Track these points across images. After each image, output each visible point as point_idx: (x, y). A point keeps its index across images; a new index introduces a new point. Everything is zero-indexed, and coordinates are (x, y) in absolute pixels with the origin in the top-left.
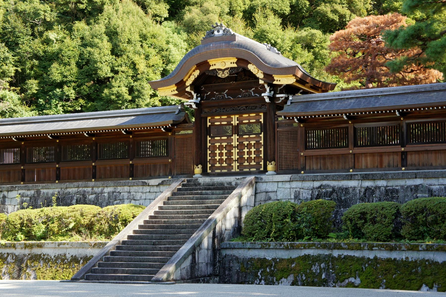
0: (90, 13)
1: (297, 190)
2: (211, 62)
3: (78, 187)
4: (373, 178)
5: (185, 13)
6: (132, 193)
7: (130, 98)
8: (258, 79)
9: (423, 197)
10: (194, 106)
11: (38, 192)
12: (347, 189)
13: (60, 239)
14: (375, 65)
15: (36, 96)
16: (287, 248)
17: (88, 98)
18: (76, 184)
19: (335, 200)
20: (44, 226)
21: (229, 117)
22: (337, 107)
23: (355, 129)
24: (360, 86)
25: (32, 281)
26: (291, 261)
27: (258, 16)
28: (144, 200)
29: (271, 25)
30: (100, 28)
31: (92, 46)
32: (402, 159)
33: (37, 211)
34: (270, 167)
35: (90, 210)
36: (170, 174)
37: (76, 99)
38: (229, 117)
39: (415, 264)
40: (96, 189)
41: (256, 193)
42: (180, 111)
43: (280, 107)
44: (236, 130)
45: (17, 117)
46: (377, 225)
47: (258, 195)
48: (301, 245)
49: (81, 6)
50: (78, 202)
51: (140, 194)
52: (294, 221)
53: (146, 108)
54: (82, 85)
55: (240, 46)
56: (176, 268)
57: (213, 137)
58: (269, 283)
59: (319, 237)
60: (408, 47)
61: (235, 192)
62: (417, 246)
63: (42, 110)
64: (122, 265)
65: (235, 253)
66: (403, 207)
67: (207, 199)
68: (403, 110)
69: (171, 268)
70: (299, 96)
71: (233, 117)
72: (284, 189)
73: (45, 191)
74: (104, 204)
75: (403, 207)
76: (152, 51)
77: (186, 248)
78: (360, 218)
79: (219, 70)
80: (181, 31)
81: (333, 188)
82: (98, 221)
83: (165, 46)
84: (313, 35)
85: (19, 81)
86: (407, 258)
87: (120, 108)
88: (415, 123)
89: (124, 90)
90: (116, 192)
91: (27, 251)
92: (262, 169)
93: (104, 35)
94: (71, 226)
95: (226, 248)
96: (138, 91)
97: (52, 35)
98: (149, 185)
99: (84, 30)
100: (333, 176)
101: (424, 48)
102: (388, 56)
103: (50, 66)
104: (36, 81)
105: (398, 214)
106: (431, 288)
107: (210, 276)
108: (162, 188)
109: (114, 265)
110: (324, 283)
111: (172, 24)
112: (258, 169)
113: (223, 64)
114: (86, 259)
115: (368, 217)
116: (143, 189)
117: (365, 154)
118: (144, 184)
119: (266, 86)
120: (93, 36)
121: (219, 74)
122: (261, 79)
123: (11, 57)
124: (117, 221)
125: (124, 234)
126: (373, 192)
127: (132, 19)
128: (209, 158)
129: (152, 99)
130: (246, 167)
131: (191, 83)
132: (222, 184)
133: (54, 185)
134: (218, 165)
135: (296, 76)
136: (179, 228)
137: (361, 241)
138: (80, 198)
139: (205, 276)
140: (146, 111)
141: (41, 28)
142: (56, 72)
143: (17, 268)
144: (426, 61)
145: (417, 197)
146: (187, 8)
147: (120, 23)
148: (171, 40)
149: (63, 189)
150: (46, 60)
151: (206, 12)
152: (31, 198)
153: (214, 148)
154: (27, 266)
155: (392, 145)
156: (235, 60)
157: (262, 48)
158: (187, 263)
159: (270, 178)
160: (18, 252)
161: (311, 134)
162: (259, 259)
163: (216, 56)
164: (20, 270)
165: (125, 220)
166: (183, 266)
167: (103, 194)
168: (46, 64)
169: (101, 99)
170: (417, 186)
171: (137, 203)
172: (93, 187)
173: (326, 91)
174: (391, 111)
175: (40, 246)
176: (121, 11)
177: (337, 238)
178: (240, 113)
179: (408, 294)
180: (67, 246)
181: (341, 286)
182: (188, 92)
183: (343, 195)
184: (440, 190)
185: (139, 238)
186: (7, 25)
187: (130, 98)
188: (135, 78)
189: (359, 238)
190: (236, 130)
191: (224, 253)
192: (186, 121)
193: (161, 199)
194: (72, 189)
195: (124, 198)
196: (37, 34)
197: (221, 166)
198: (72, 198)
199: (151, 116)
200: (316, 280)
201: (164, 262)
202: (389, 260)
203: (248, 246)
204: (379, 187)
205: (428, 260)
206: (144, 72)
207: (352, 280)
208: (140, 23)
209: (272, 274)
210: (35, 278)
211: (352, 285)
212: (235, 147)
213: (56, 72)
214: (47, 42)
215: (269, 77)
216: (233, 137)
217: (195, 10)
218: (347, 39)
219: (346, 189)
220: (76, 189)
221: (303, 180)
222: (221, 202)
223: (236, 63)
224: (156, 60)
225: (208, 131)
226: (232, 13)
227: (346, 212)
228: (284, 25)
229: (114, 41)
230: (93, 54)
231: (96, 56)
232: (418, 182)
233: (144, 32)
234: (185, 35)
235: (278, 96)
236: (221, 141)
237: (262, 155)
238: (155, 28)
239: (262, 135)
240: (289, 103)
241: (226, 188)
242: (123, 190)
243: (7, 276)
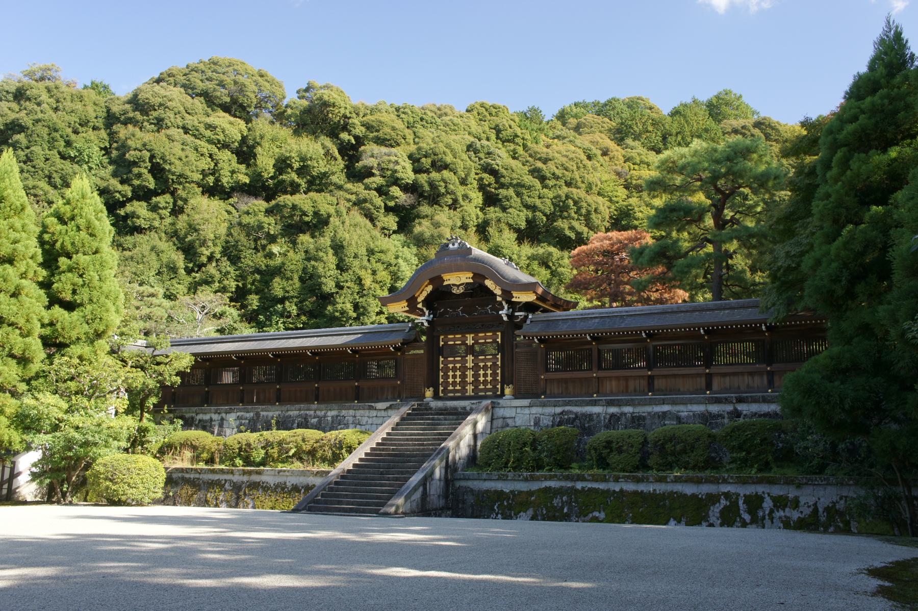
0: (315, 226)
2: (445, 277)
3: (300, 410)
4: (618, 404)
5: (414, 226)
7: (355, 315)
8: (495, 295)
9: (670, 424)
10: (426, 324)
11: (258, 414)
13: (280, 466)
14: (619, 283)
15: (256, 313)
16: (526, 480)
17: (311, 314)
18: (297, 406)
19: (578, 427)
20: (263, 452)
21: (463, 336)
22: (580, 327)
23: (599, 351)
25: (250, 510)
26: (530, 493)
27: (491, 230)
29: (507, 239)
30: (325, 241)
31: (316, 260)
32: (649, 384)
33: (255, 435)
34: (508, 391)
35: (313, 435)
36: (399, 397)
37: (298, 315)
38: (463, 336)
39: (663, 496)
40: (318, 413)
41: (492, 419)
42: (411, 329)
43: (519, 326)
44: (470, 350)
45: (237, 334)
46: (623, 455)
47: (494, 422)
48: (542, 476)
49: (307, 219)
50: (298, 427)
51: (366, 419)
52: (534, 449)
53: (372, 326)
54: (304, 300)
55: (477, 260)
56: (406, 501)
57: (446, 358)
58: (505, 517)
59: (561, 467)
60: (653, 266)
61: (469, 418)
62: (666, 477)
63: (262, 327)
64: (346, 496)
65: (470, 484)
66: (651, 436)
67: (440, 425)
69: (400, 501)
70: (539, 315)
71: (468, 335)
74: (328, 429)
75: (651, 436)
76: (380, 267)
77: (415, 479)
78: (605, 447)
79: (454, 285)
80: (411, 245)
81: (576, 414)
82: (321, 447)
83: (393, 261)
84: (550, 254)
85: (239, 297)
86: (655, 490)
87: (344, 326)
88: (662, 346)
89: (349, 306)
91: (245, 478)
93: (329, 249)
94: (291, 454)
95: (460, 479)
96: (363, 307)
97: (275, 249)
99: (309, 243)
100: (576, 401)
101: (669, 267)
102: (631, 274)
103: (271, 281)
104: (257, 297)
105: (645, 442)
106: (679, 522)
107: (442, 509)
108: (390, 412)
109: (338, 496)
110: (566, 518)
111: (401, 237)
112: (495, 393)
113: (458, 280)
114: (308, 488)
115: (614, 445)
117: (610, 378)
118: (371, 408)
119: (504, 303)
120: (318, 250)
123: (232, 271)
124: (341, 448)
125: (349, 462)
126: (619, 419)
127: (359, 232)
128: (441, 380)
129: (378, 317)
130: (481, 390)
132: (456, 409)
133: (274, 408)
134: (451, 388)
135: (537, 294)
136: (408, 456)
137: (606, 472)
139: (436, 509)
141: (264, 242)
142: (278, 287)
143: (235, 496)
144: (671, 280)
145: (665, 425)
146: (417, 221)
147: (347, 236)
148: (400, 254)
150: (268, 274)
151: (437, 225)
153: (446, 370)
154: (245, 494)
155: (635, 368)
156: (471, 275)
157: (499, 262)
158: (418, 495)
159: (508, 403)
160: (236, 478)
161: (547, 354)
162: (496, 491)
163: (450, 270)
164: (238, 498)
165: (350, 447)
166: (413, 498)
168: (267, 278)
169: (325, 316)
170: (664, 413)
171: (363, 428)
172: (315, 411)
173: (568, 310)
174: (636, 333)
175: (259, 473)
176: (347, 223)
177: (580, 468)
178: (475, 331)
179: (657, 529)
180: (287, 473)
181: (584, 521)
182: (419, 309)
184: (688, 417)
185: (365, 466)
186: (230, 239)
187: (355, 315)
188: (361, 293)
189: (604, 469)
190: (470, 350)
191: (458, 484)
192: (417, 340)
193: (389, 424)
194: (293, 412)
196: (259, 248)
198: (293, 422)
200: (557, 514)
201: (392, 494)
202: (635, 493)
203: (484, 476)
204: (625, 414)
205: (676, 493)
206: (370, 288)
207: (596, 514)
208: (367, 237)
209: (510, 507)
210: (254, 507)
211: (596, 520)
213: (278, 287)
214: (270, 255)
215: (507, 294)
217: (426, 223)
218: (589, 255)
221: (544, 405)
222: (455, 429)
224: (383, 275)
225: (440, 351)
226: (464, 227)
227: (590, 440)
228: (520, 241)
229: (340, 255)
230: (317, 269)
231: (321, 270)
232: (666, 408)
233: (372, 246)
234: (414, 249)
235: (516, 314)
236: (455, 362)
237: (499, 378)
238: (384, 243)
239: (499, 356)
240: (528, 322)
241: (460, 414)
242: (348, 414)
243: (224, 504)
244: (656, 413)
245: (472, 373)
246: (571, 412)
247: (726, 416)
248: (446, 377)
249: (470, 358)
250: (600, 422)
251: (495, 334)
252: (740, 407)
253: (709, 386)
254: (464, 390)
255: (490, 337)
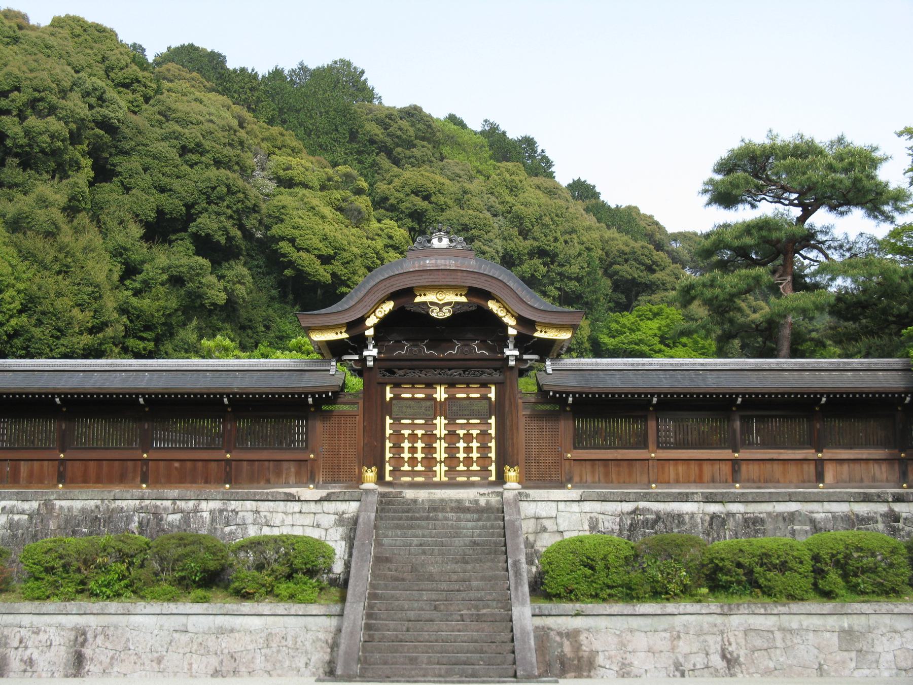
1: (592, 515)
6: (262, 514)
12: (680, 516)
28: (290, 527)
34: (512, 474)
40: (181, 504)
51: (280, 516)
68: (320, 395)
72: (569, 514)
73: (65, 504)
81: (658, 514)
90: (227, 511)
98: (299, 501)
116: (286, 506)
121: (432, 311)
122: (511, 326)
126: (724, 522)
130: (461, 473)
131: (376, 321)
132: (459, 501)
138: (149, 520)
140: (283, 365)
149: (106, 502)
152: (31, 516)
153: (398, 437)
167: (199, 514)
170: (792, 514)
183: (674, 525)
184: (826, 520)
195: (247, 522)
197: (413, 471)
204: (734, 515)
212: (440, 439)
216: (436, 422)
219: (679, 515)
220: (138, 502)
225: (386, 408)
232: (793, 507)
236: (413, 426)
237: (493, 455)
244: (779, 515)
245: (444, 445)
246: (649, 510)
247: (880, 519)
248: (397, 447)
249: (440, 422)
250: (695, 526)
252: (898, 507)
253: (820, 477)
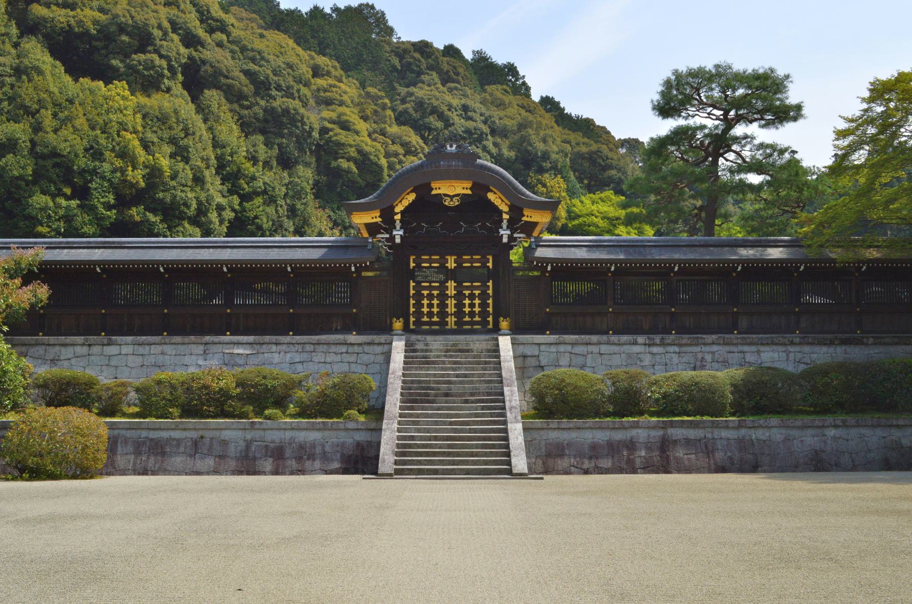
24: (49, 233)
34: (504, 324)
71: (449, 257)
92: (491, 326)
122: (506, 213)
153: (419, 297)
156: (469, 185)
199: (658, 249)
203: (555, 425)
216: (448, 284)
223: (470, 189)
237: (490, 309)
245: (454, 302)
248: (419, 305)
249: (451, 284)
251: (484, 257)
254: (443, 323)
255: (477, 261)
